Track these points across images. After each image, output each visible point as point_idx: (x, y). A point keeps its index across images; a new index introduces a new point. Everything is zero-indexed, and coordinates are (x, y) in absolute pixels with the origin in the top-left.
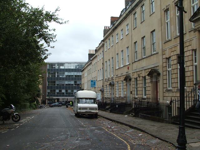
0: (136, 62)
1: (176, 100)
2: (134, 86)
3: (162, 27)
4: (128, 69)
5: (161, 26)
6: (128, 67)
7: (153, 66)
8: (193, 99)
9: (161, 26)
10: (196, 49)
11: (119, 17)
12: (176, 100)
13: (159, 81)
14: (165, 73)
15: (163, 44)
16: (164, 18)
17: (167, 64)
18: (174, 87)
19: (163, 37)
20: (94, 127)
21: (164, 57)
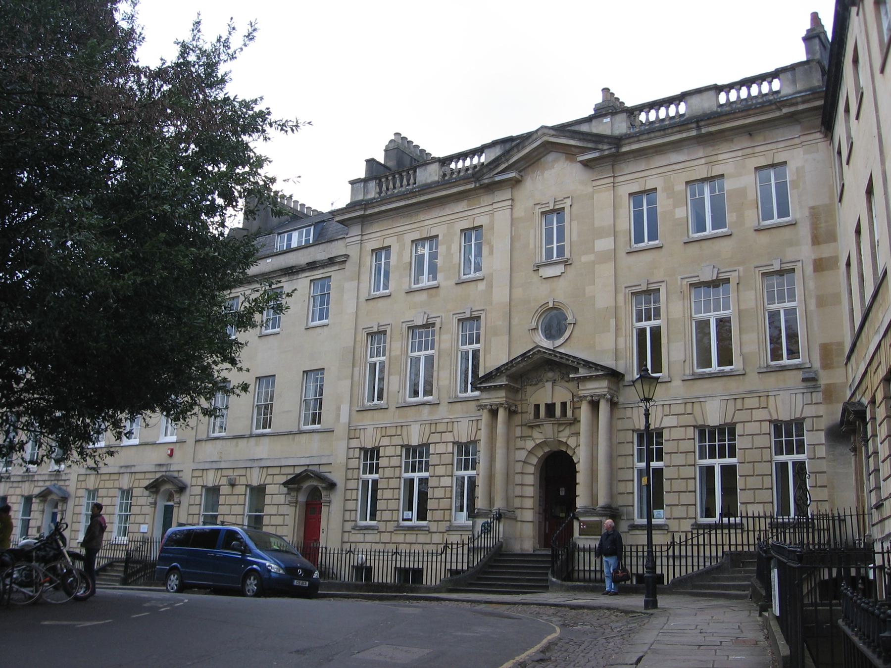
0: (301, 432)
1: (437, 553)
2: (200, 510)
3: (356, 369)
4: (171, 455)
5: (353, 366)
6: (172, 450)
7: (307, 462)
8: (768, 520)
9: (353, 366)
10: (475, 442)
11: (595, 241)
12: (437, 553)
13: (330, 502)
14: (352, 484)
15: (354, 413)
16: (364, 349)
17: (362, 462)
18: (387, 521)
19: (688, 355)
20: (178, 606)
21: (355, 443)
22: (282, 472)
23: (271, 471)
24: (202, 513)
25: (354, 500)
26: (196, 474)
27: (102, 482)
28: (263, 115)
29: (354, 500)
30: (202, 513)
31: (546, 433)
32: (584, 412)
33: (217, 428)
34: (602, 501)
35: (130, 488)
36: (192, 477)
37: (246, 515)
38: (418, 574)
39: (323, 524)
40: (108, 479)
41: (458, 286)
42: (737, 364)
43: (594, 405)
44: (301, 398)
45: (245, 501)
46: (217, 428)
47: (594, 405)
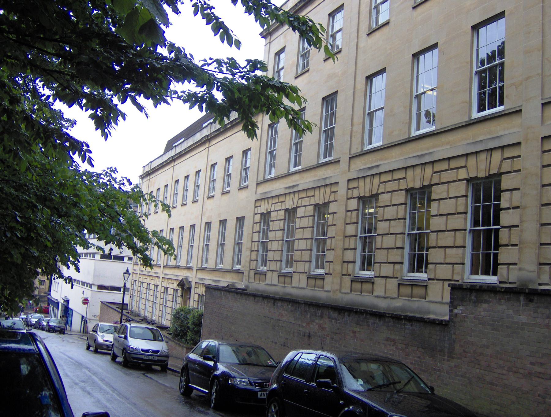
20: (109, 322)
22: (452, 167)
23: (438, 167)
24: (407, 232)
25: (353, 223)
26: (352, 185)
27: (382, 186)
28: (185, 101)
29: (353, 223)
30: (359, 235)
33: (423, 119)
35: (491, 176)
36: (349, 189)
37: (359, 237)
38: (374, 379)
39: (499, 258)
40: (390, 179)
41: (371, 36)
44: (364, 112)
45: (313, 224)
46: (423, 119)
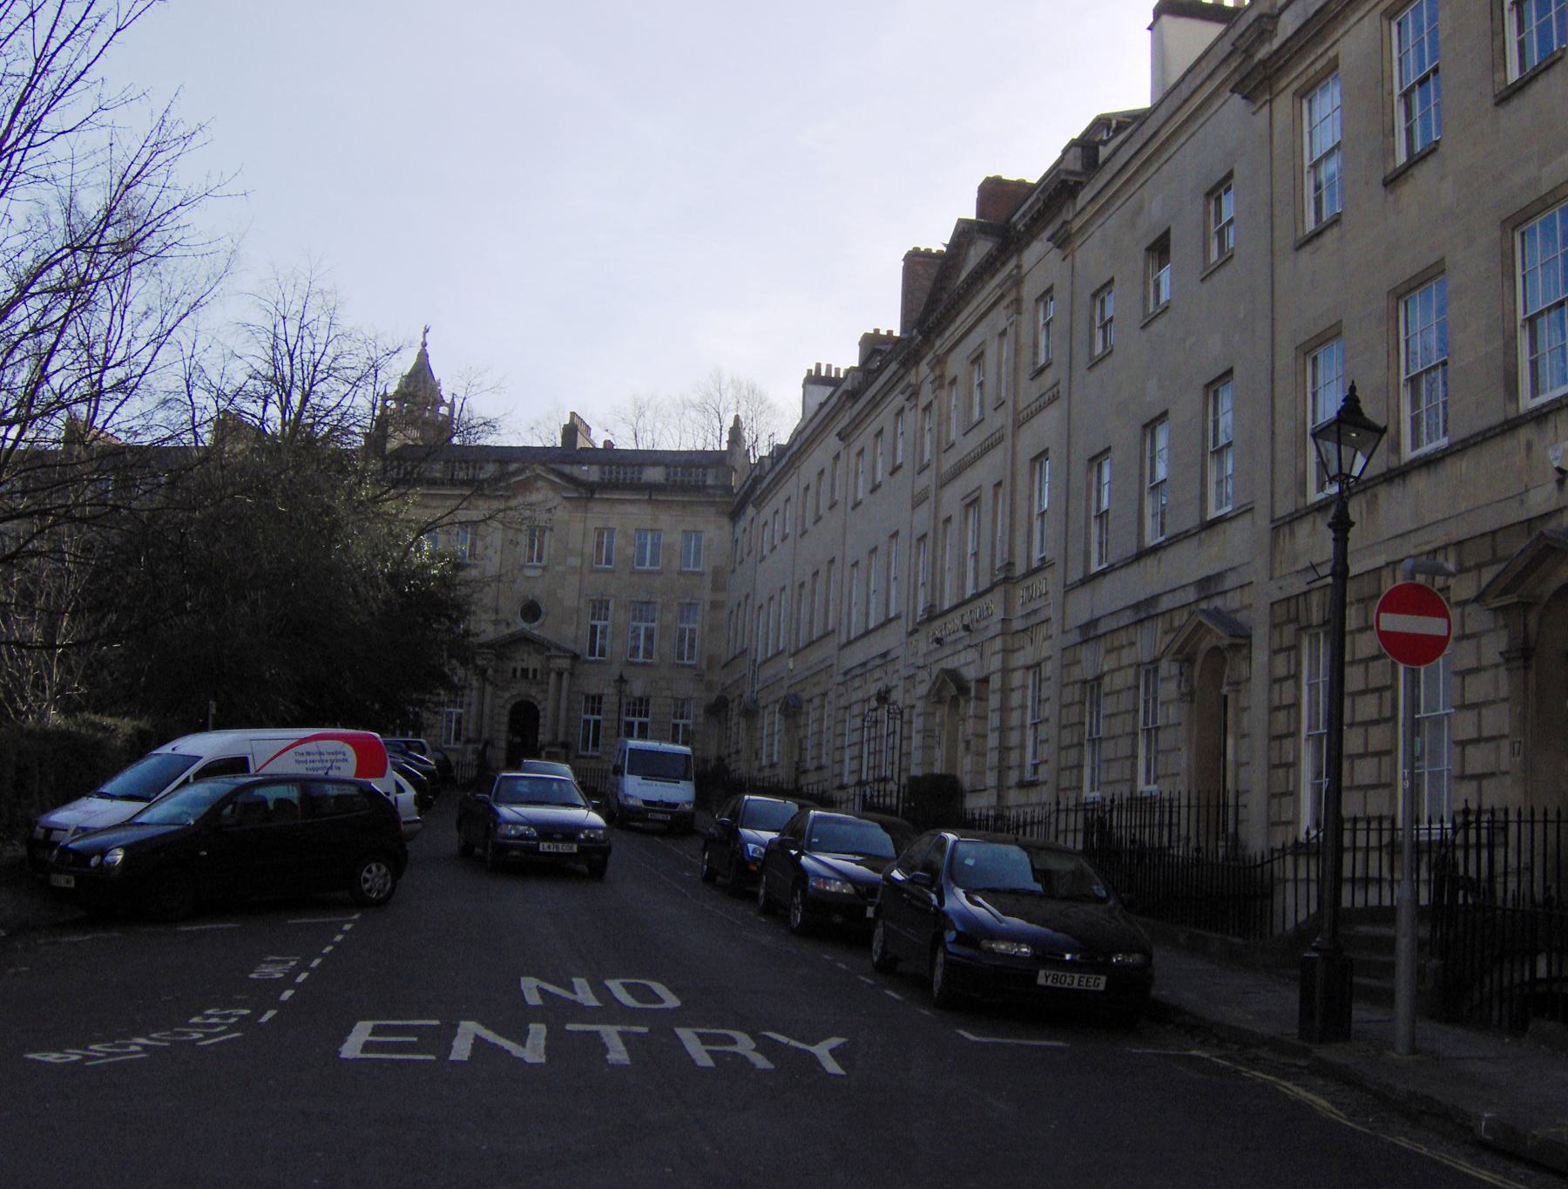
31: (520, 689)
32: (553, 676)
34: (561, 738)
42: (655, 659)
43: (560, 675)
47: (560, 675)
